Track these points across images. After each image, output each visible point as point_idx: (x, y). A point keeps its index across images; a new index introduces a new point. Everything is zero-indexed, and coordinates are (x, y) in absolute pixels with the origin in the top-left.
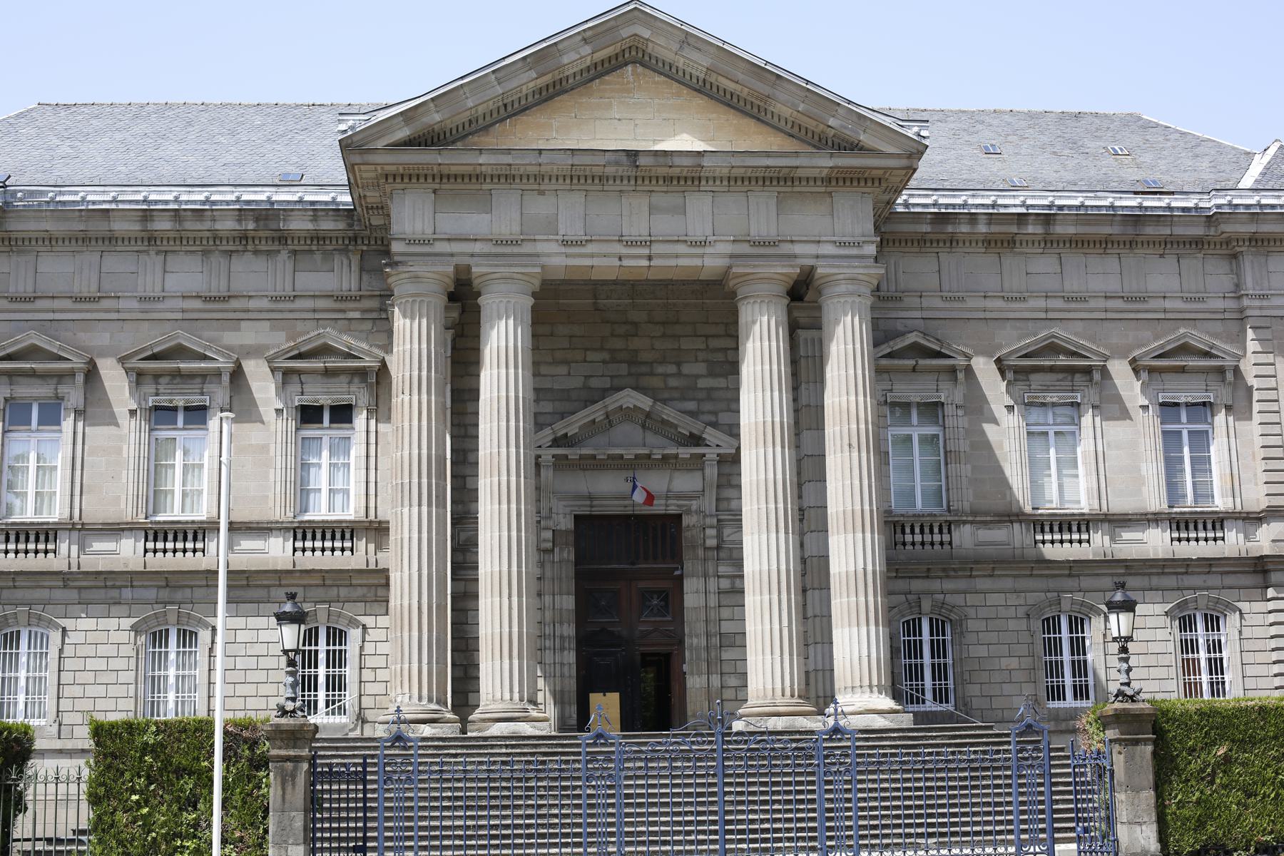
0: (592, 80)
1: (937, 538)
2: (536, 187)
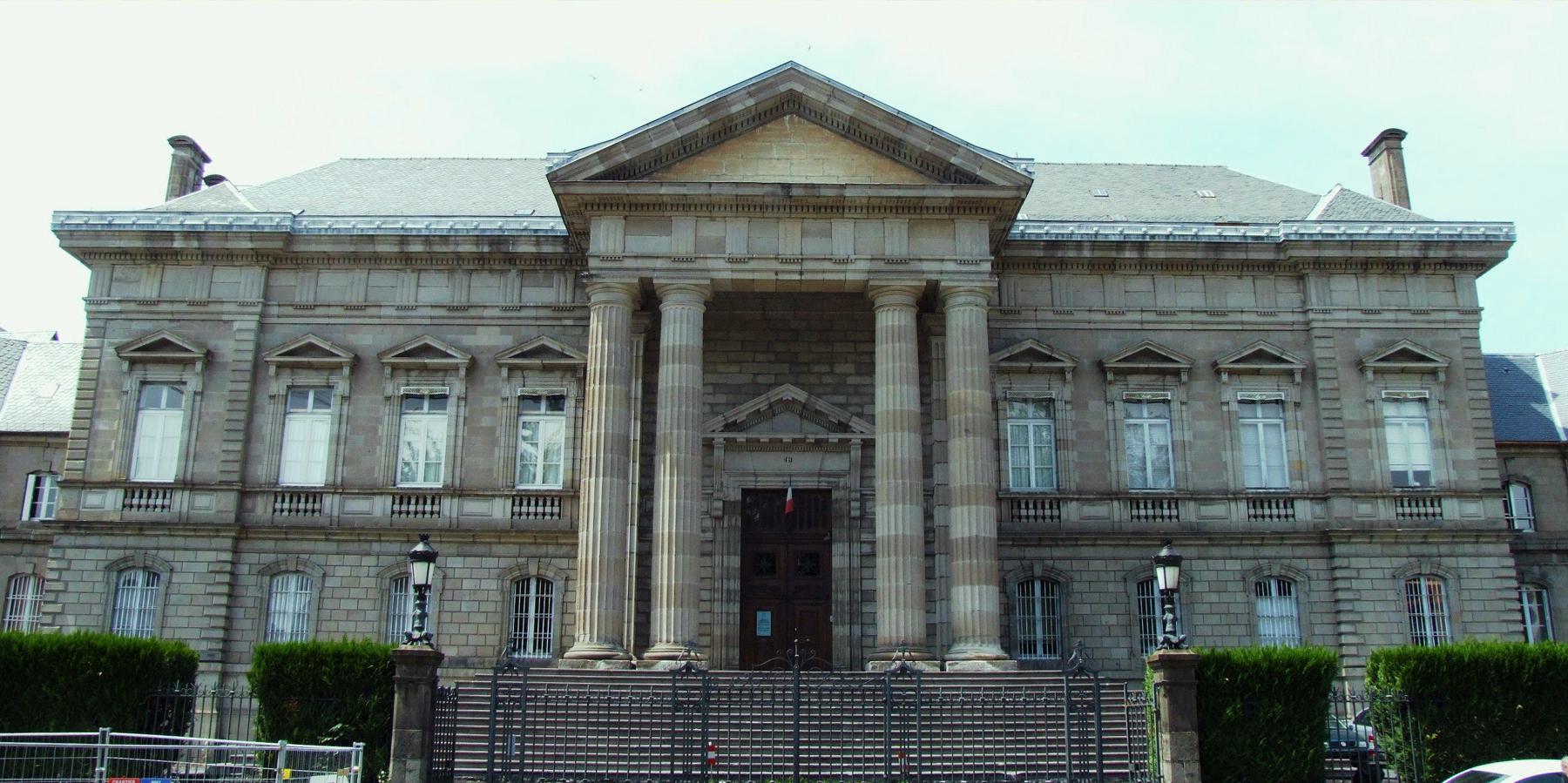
1: (1048, 512)
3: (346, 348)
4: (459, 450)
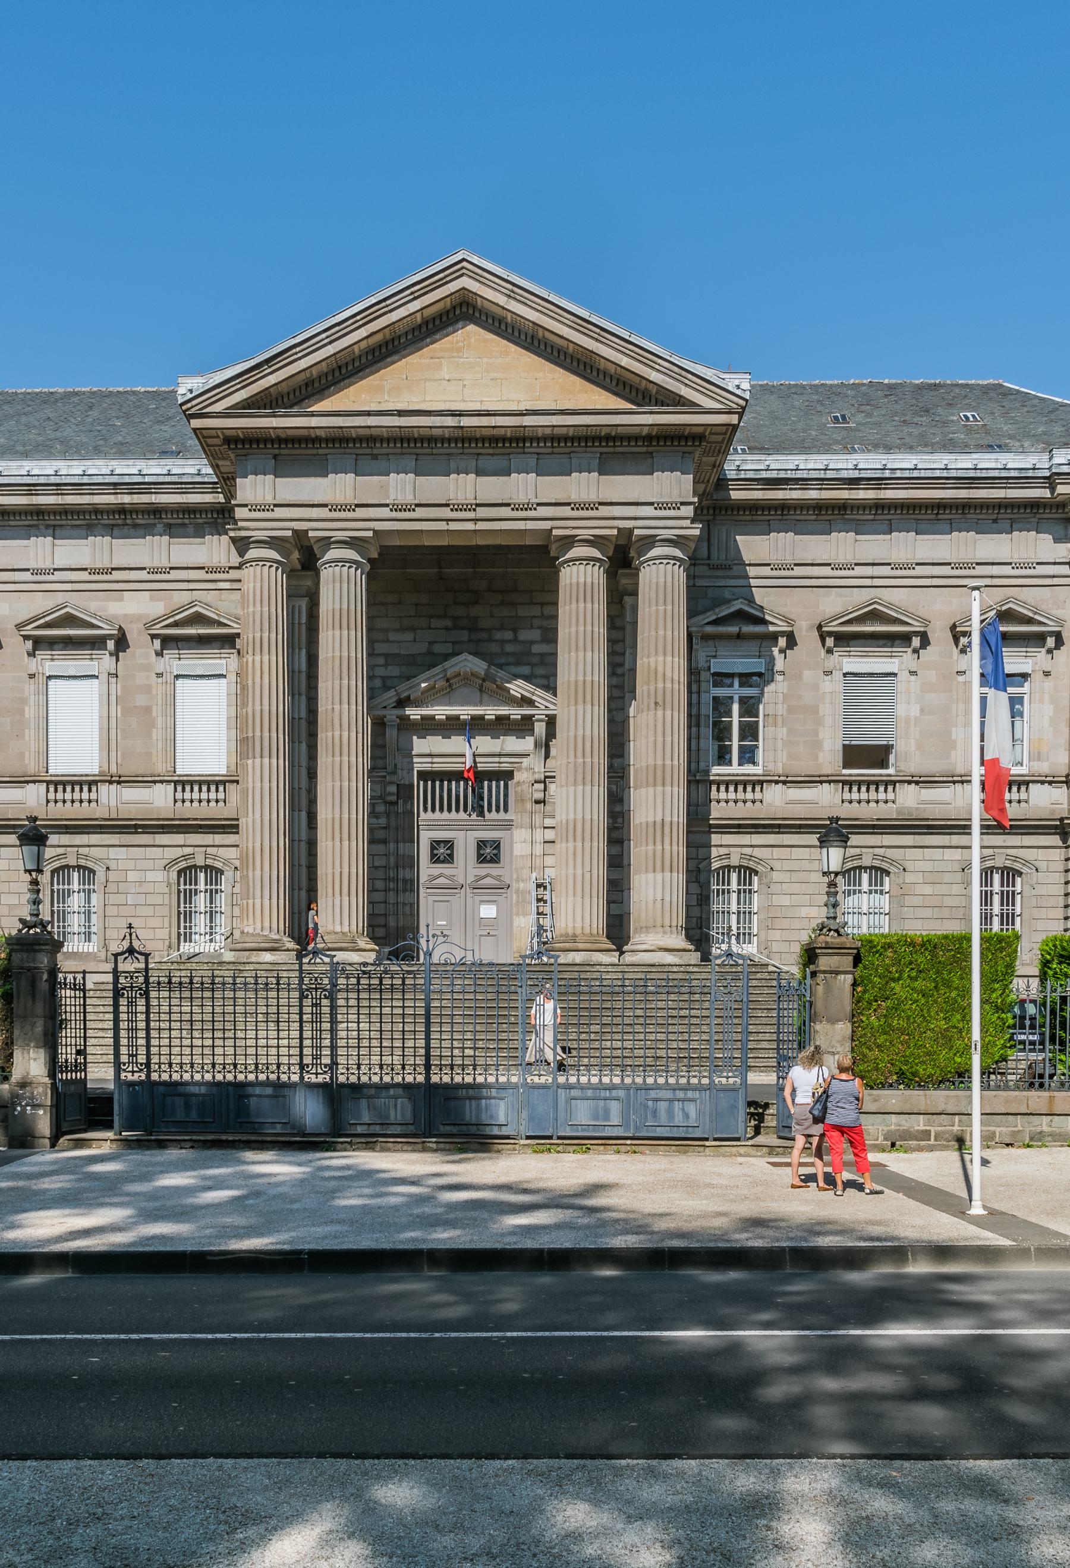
2: (368, 451)
3: (107, 621)
4: (113, 732)
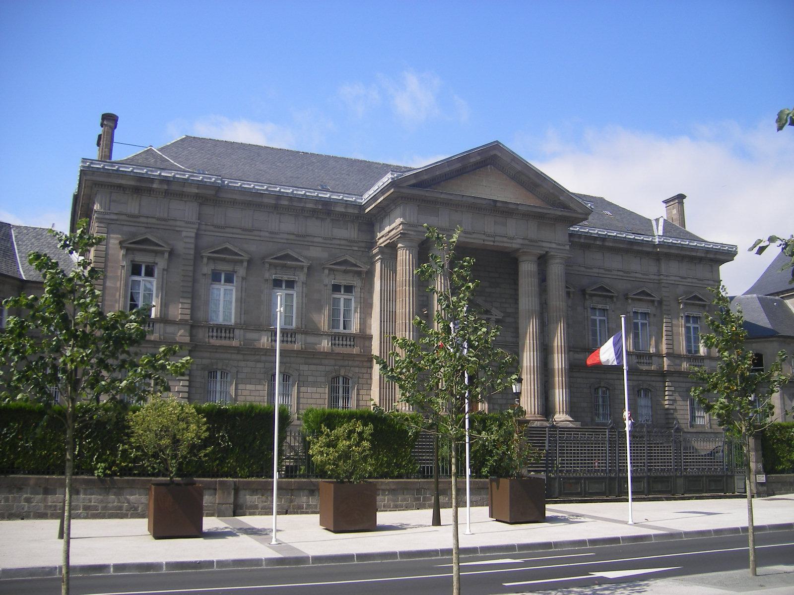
0: (475, 169)
